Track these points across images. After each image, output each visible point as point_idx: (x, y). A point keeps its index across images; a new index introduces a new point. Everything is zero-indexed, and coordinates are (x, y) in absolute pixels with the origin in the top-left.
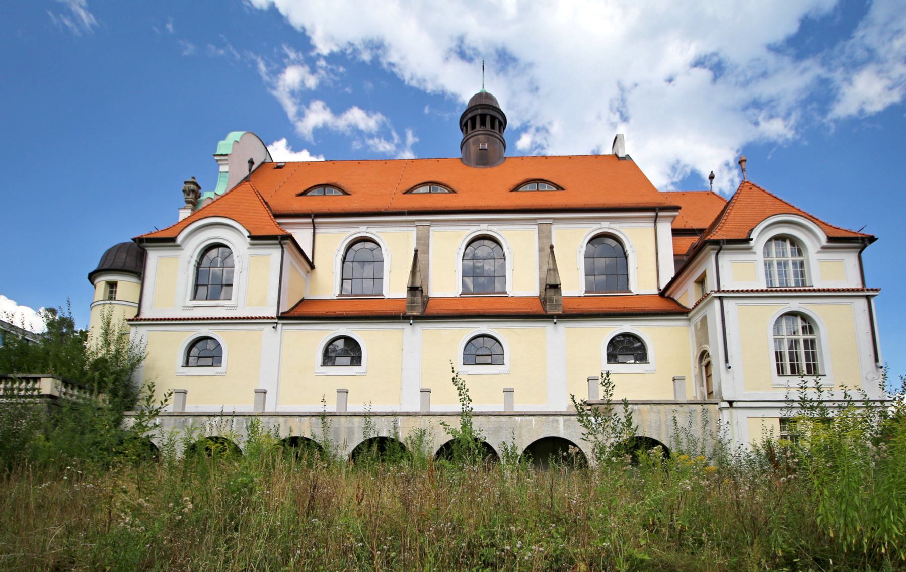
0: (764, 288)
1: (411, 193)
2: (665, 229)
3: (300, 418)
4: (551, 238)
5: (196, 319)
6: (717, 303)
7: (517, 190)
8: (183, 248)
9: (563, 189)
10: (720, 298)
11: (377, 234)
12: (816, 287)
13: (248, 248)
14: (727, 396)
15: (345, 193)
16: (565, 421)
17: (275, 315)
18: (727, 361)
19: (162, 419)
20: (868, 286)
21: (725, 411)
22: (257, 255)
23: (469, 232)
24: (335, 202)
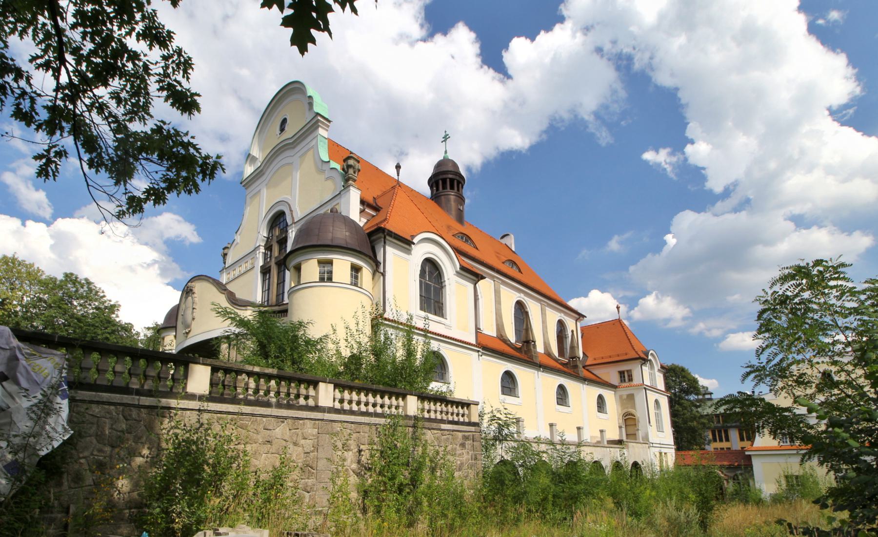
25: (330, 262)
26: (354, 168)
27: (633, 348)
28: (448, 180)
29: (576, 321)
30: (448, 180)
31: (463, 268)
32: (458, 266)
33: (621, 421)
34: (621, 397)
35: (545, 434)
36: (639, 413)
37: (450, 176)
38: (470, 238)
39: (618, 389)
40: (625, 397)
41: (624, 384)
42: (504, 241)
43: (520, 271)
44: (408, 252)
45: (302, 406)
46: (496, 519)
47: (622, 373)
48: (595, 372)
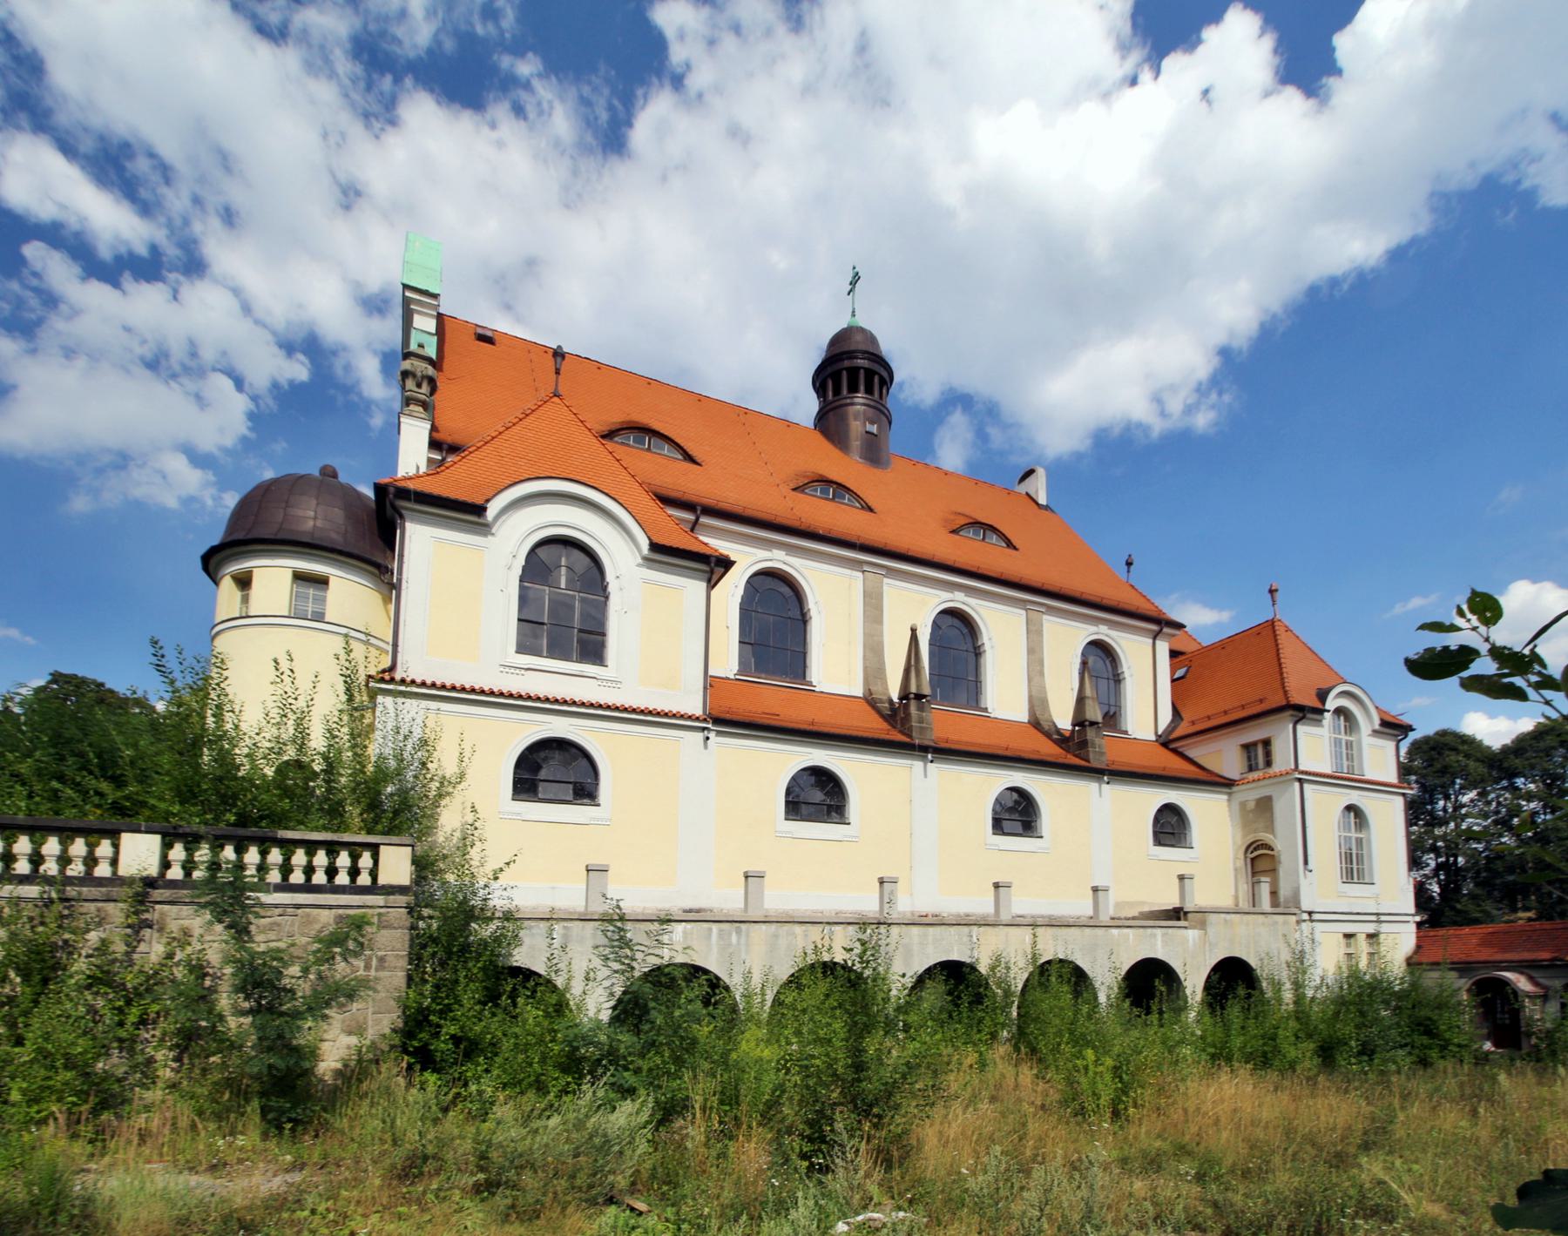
0: (1328, 771)
1: (803, 492)
2: (1163, 648)
3: (804, 927)
4: (1042, 635)
5: (600, 706)
6: (1297, 785)
7: (611, 439)
8: (493, 531)
9: (1015, 548)
10: (1300, 780)
11: (802, 570)
12: (1368, 776)
13: (639, 565)
14: (1306, 906)
15: (689, 458)
16: (1163, 935)
17: (699, 712)
18: (1306, 862)
19: (565, 927)
20: (1301, 768)
21: (1304, 924)
22: (655, 583)
23: (754, 559)
24: (989, 555)
25: (322, 582)
26: (414, 375)
27: (1283, 684)
28: (862, 371)
29: (1155, 638)
30: (862, 371)
31: (655, 547)
32: (644, 544)
33: (1240, 863)
34: (1243, 805)
35: (571, 895)
36: (1284, 842)
37: (860, 362)
38: (848, 490)
39: (1235, 789)
40: (1252, 805)
41: (1255, 775)
42: (1022, 488)
43: (1010, 544)
44: (484, 529)
45: (339, 886)
46: (54, 1098)
47: (1248, 748)
48: (1192, 753)
